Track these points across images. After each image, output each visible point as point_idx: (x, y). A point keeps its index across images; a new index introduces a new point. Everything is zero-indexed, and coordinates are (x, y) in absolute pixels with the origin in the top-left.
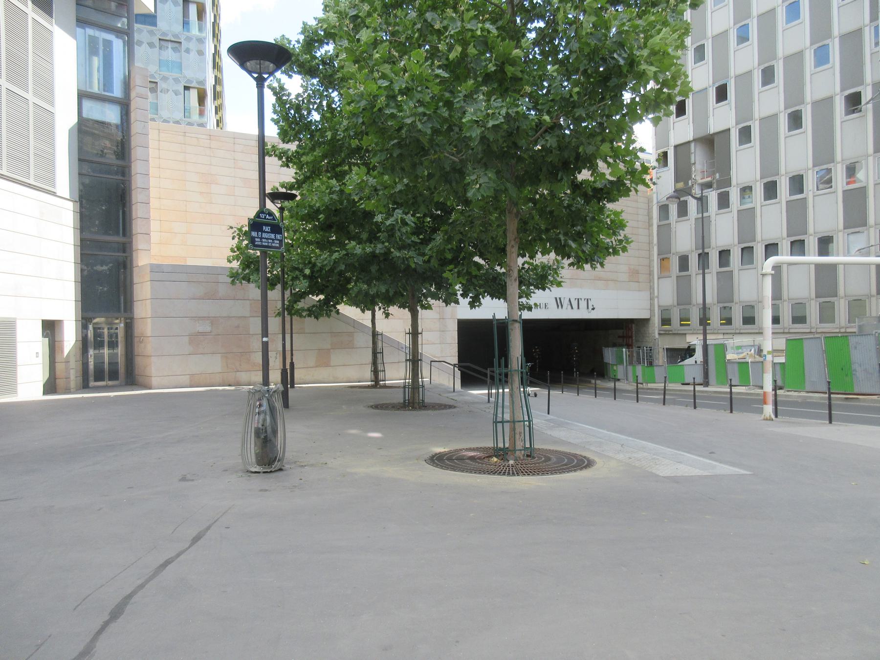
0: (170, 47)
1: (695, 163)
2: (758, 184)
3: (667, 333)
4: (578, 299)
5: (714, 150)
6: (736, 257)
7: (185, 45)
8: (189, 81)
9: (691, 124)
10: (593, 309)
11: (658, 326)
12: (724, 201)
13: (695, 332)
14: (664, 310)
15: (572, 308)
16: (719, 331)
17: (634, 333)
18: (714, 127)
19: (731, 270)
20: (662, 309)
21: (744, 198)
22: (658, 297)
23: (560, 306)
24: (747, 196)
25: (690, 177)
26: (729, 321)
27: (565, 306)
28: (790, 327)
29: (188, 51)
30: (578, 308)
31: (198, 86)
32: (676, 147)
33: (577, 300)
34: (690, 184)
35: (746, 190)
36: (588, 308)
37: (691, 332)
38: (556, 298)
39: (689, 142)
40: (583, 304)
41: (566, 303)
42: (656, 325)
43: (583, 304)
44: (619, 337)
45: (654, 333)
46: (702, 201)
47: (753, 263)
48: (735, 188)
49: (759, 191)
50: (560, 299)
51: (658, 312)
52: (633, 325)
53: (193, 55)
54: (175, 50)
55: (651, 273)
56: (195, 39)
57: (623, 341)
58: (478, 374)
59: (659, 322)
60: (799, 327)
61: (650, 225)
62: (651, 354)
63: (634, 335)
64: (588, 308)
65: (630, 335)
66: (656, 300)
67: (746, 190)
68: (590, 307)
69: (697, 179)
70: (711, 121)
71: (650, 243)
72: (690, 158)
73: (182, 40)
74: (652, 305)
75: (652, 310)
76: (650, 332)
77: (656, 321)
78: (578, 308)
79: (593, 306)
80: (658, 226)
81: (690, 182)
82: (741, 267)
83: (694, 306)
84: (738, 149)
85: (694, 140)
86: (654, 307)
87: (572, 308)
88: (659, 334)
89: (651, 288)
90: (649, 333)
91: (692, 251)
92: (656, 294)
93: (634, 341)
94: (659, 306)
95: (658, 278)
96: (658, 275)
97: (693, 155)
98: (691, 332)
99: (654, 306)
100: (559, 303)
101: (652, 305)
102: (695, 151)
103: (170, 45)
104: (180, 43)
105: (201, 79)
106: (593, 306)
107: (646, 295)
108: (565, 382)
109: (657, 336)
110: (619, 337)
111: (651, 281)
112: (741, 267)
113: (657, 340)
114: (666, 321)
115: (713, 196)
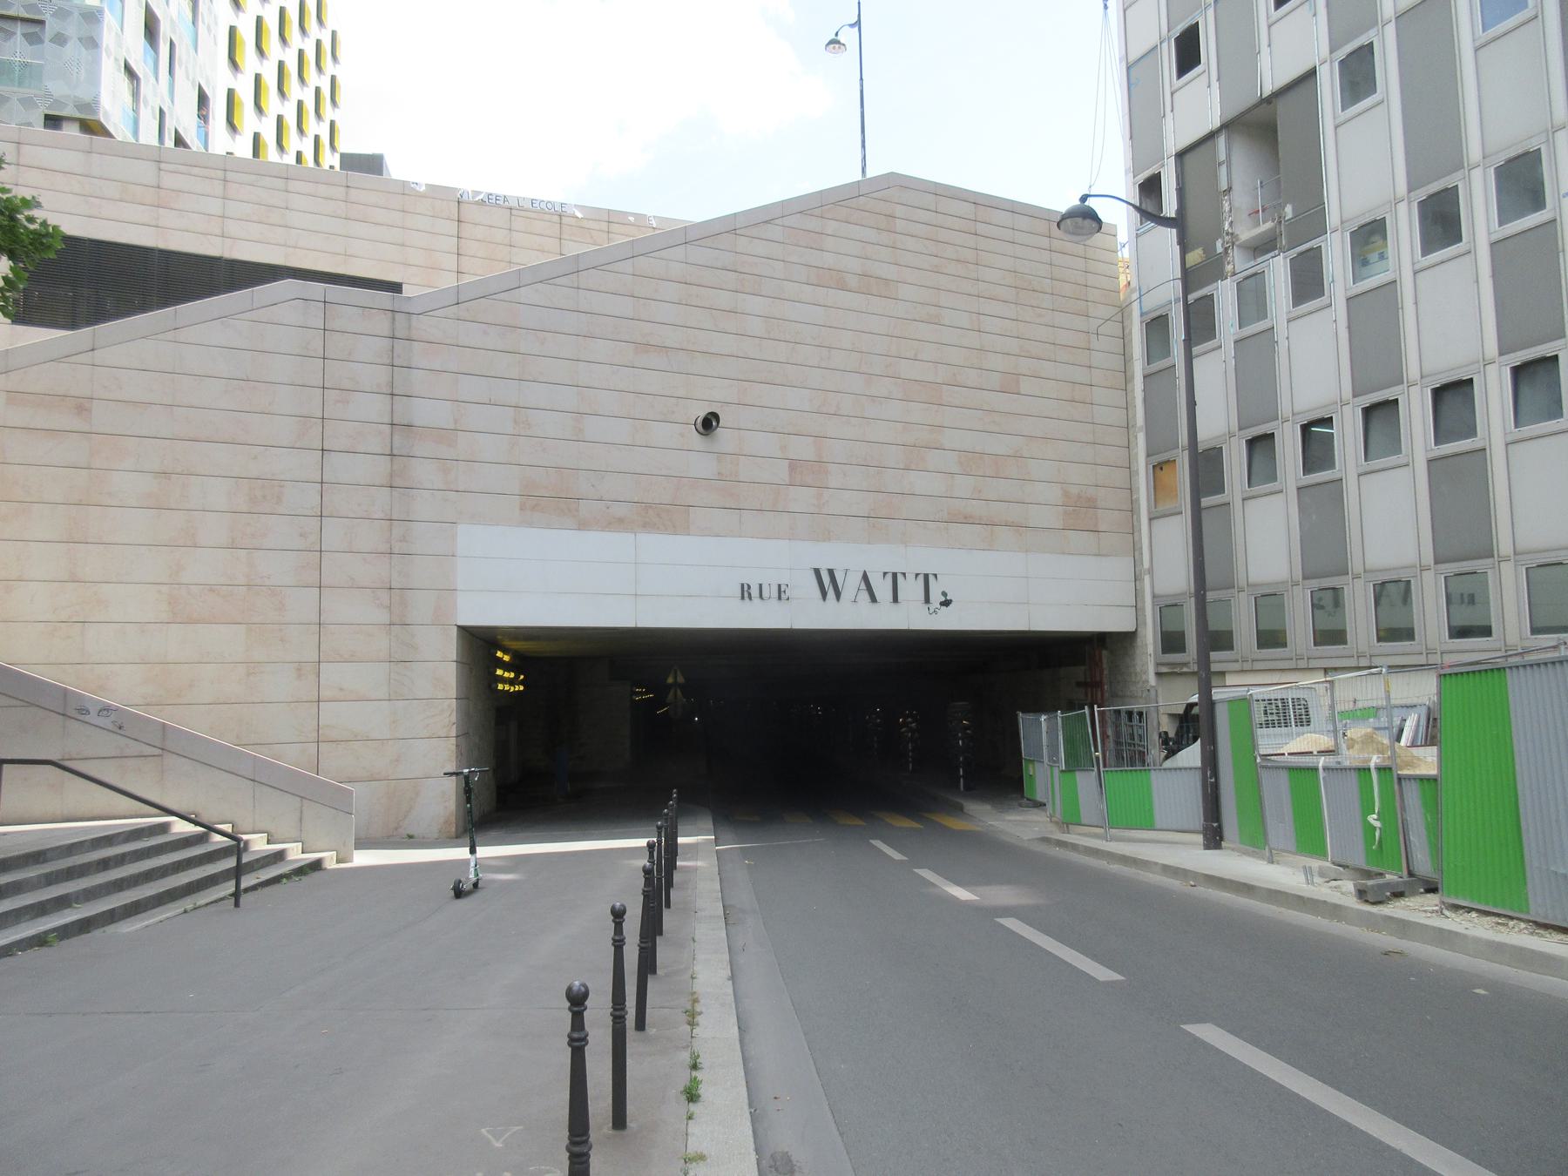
0: (19, 33)
1: (1230, 189)
2: (1402, 208)
3: (1177, 670)
4: (895, 575)
5: (1277, 153)
6: (1348, 433)
7: (52, 26)
8: (58, 103)
9: (1215, 85)
10: (946, 603)
11: (1155, 651)
12: (1308, 282)
13: (1247, 666)
14: (1167, 608)
15: (873, 599)
16: (1313, 664)
17: (1106, 672)
18: (1273, 74)
19: (1337, 476)
20: (1163, 604)
21: (1365, 263)
22: (1151, 571)
23: (831, 593)
24: (1374, 257)
25: (1218, 232)
26: (1331, 636)
27: (847, 594)
28: (1445, 648)
29: (60, 40)
30: (895, 599)
31: (78, 115)
32: (1181, 155)
33: (889, 577)
34: (1220, 249)
35: (1369, 236)
36: (927, 600)
37: (1237, 666)
38: (817, 572)
39: (1211, 136)
40: (911, 590)
41: (851, 585)
42: (1150, 649)
43: (911, 590)
44: (1079, 684)
45: (1146, 672)
46: (1253, 298)
47: (1398, 450)
48: (1337, 235)
49: (1405, 229)
50: (831, 572)
51: (1153, 609)
52: (1105, 653)
53: (72, 49)
54: (33, 39)
55: (1133, 510)
56: (76, 14)
57: (1086, 695)
58: (135, 852)
59: (1155, 642)
60: (1473, 649)
61: (1128, 379)
62: (1140, 732)
63: (1105, 680)
64: (927, 600)
65: (1098, 679)
66: (1147, 579)
67: (1369, 236)
68: (936, 597)
69: (1237, 232)
70: (1264, 61)
71: (1129, 426)
72: (1215, 177)
73: (47, 17)
74: (1138, 594)
75: (1138, 608)
76: (1138, 670)
77: (1149, 640)
78: (895, 599)
79: (944, 594)
80: (1145, 377)
81: (1219, 244)
82: (1366, 466)
83: (1241, 590)
84: (1418, 267)
85: (1226, 126)
86: (1144, 602)
87: (873, 599)
88: (1158, 674)
89: (1136, 549)
90: (1136, 674)
91: (1231, 435)
92: (1146, 565)
93: (1106, 695)
94: (1154, 596)
95: (1150, 520)
96: (1149, 512)
97: (1224, 169)
98: (1237, 666)
99: (1143, 596)
100: (827, 585)
101: (1138, 594)
102: (1229, 156)
103: (19, 29)
104: (41, 23)
105: (87, 98)
106: (944, 594)
107: (1121, 567)
108: (968, 788)
109: (1152, 680)
110: (1079, 684)
111: (1134, 530)
112: (1366, 466)
113: (1153, 692)
114: (1171, 642)
115: (1278, 270)
